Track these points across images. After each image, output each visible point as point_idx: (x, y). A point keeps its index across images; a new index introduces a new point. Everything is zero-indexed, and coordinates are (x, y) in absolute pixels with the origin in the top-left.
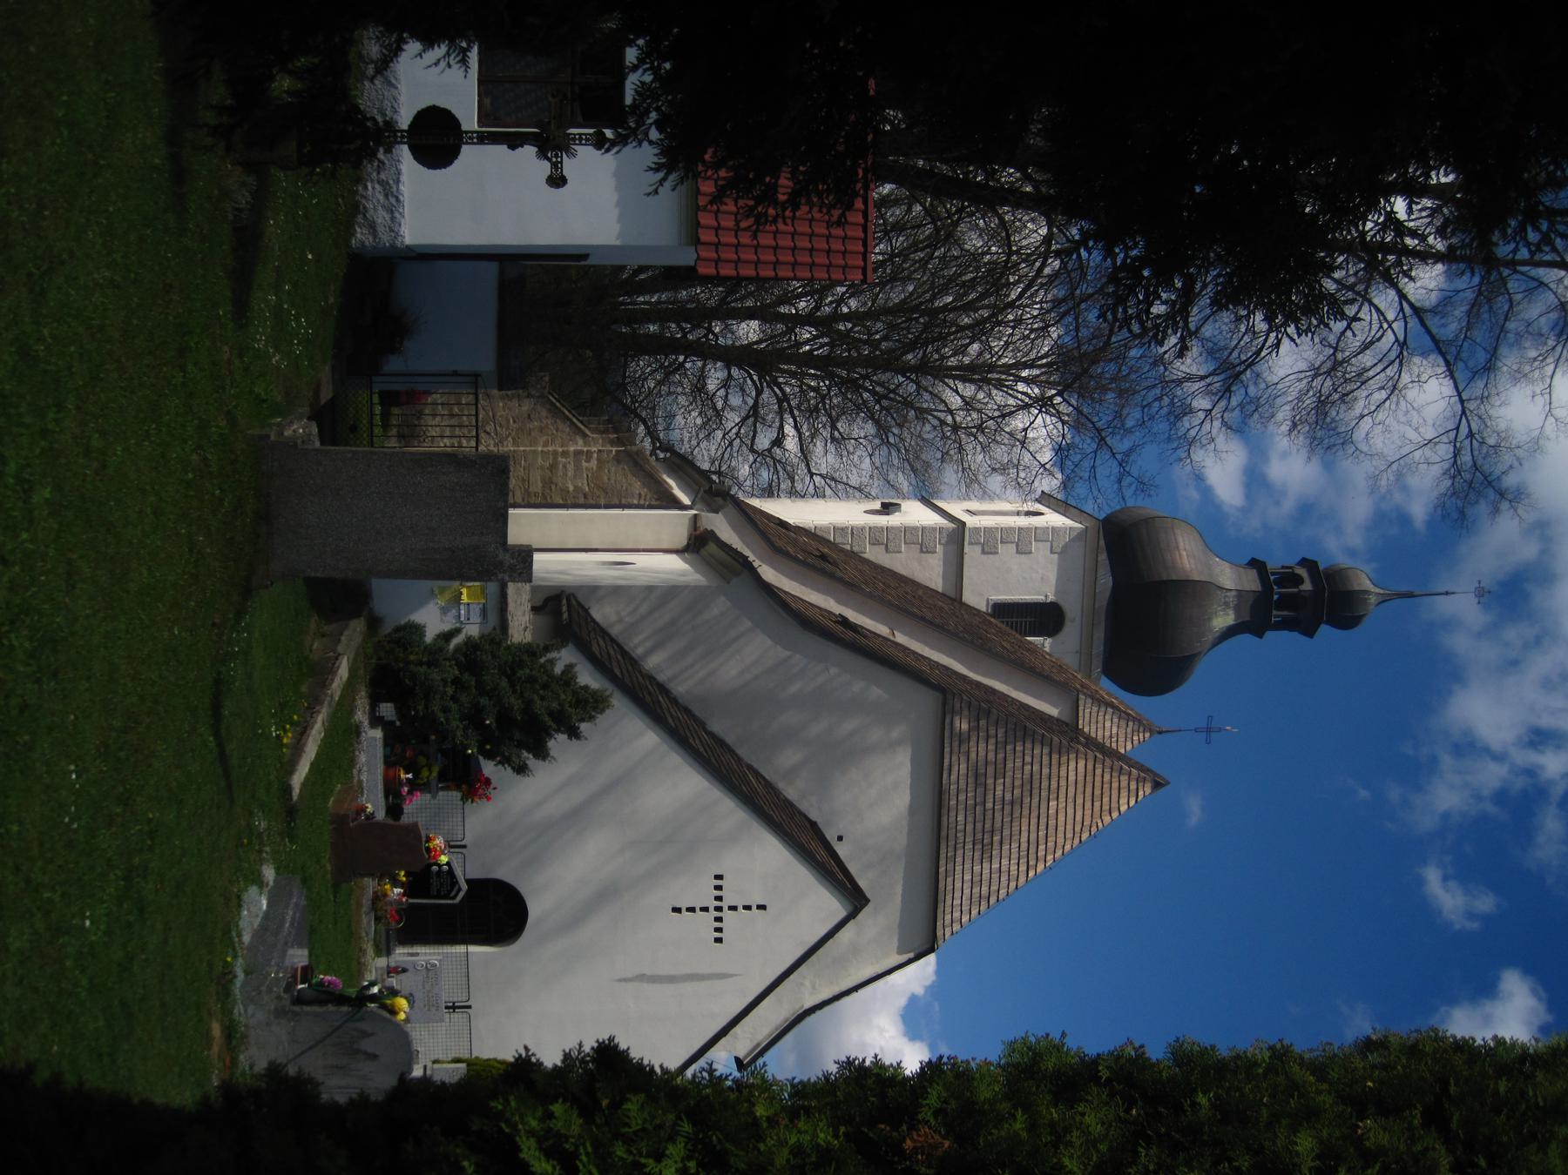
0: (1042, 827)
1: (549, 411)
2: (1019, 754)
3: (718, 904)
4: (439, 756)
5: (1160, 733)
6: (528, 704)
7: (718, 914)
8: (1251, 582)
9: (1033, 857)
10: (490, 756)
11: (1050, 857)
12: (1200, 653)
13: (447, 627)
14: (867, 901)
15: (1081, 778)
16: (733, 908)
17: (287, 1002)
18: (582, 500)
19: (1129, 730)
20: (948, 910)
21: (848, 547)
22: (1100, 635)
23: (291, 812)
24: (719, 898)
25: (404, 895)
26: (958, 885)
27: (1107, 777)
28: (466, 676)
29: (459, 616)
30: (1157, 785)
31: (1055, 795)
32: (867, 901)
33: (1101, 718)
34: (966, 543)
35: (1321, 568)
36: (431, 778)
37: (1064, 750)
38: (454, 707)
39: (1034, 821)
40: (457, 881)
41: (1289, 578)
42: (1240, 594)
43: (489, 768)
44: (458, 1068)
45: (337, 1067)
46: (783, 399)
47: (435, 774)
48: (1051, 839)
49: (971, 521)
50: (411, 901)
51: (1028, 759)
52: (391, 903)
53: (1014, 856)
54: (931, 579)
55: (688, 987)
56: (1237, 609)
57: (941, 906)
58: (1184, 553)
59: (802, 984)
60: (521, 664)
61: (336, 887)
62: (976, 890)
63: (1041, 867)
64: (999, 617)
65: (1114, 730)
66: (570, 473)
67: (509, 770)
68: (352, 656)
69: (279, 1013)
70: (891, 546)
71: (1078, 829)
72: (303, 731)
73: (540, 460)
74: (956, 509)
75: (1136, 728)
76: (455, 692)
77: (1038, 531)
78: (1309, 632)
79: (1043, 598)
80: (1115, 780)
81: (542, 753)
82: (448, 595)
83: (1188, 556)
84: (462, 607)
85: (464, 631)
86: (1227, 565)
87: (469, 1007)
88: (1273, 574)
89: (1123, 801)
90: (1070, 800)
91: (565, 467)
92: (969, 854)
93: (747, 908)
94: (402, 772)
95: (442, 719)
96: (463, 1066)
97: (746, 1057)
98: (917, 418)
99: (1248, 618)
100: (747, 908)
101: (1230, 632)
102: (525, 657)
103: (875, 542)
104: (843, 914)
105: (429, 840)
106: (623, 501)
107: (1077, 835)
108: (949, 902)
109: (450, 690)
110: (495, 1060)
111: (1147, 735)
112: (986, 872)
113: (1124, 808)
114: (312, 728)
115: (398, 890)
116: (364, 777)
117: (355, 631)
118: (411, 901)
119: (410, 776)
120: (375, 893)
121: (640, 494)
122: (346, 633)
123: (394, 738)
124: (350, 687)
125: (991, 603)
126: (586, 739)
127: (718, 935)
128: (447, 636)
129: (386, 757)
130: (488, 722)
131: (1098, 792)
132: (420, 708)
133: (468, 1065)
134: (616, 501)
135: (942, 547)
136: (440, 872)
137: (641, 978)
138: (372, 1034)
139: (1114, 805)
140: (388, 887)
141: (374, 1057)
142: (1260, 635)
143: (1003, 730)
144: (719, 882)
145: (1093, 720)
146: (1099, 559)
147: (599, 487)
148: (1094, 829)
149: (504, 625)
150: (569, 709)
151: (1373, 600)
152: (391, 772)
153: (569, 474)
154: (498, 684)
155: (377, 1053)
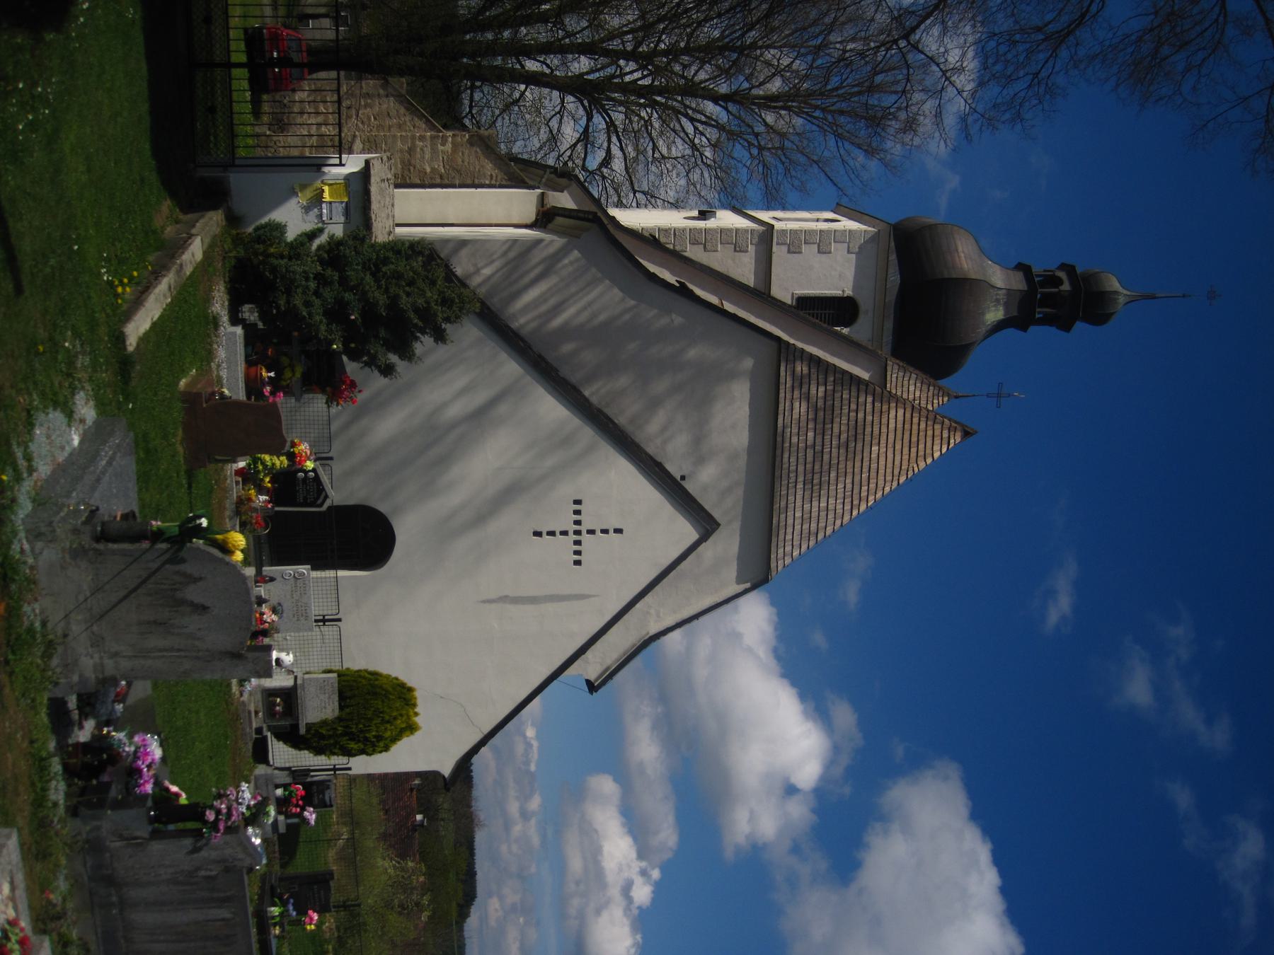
0: (865, 470)
1: (407, 109)
2: (846, 402)
3: (577, 527)
4: (303, 357)
5: (956, 397)
6: (394, 300)
7: (577, 538)
8: (1018, 282)
9: (856, 497)
10: (354, 356)
11: (871, 498)
12: (973, 344)
13: (309, 227)
14: (718, 525)
15: (900, 426)
16: (591, 532)
17: (86, 540)
18: (438, 181)
19: (930, 394)
20: (781, 544)
21: (671, 247)
22: (889, 325)
23: (124, 364)
24: (578, 523)
25: (269, 502)
26: (790, 521)
27: (923, 425)
28: (329, 272)
29: (321, 216)
30: (966, 434)
31: (877, 441)
32: (718, 525)
33: (906, 383)
34: (774, 243)
35: (1078, 272)
36: (294, 379)
37: (885, 399)
38: (317, 302)
39: (858, 464)
40: (323, 489)
41: (1053, 281)
42: (1009, 292)
43: (352, 368)
44: (329, 678)
45: (155, 622)
46: (611, 126)
47: (298, 375)
48: (873, 481)
49: (778, 226)
50: (277, 509)
51: (853, 406)
52: (255, 510)
53: (840, 495)
54: (743, 275)
55: (550, 608)
56: (1007, 306)
57: (774, 539)
58: (962, 255)
59: (648, 613)
60: (386, 261)
61: (190, 475)
62: (806, 526)
63: (863, 507)
64: (806, 310)
65: (917, 394)
66: (427, 156)
67: (376, 372)
68: (207, 241)
69: (78, 553)
70: (709, 246)
71: (896, 472)
72: (144, 290)
73: (399, 143)
74: (765, 216)
75: (936, 392)
76: (318, 287)
77: (837, 234)
78: (1067, 327)
79: (841, 292)
80: (930, 428)
81: (406, 352)
82: (309, 193)
83: (965, 257)
84: (324, 205)
85: (326, 231)
86: (997, 267)
87: (339, 620)
88: (1037, 276)
89: (936, 448)
90: (890, 445)
91: (422, 149)
92: (800, 493)
93: (605, 531)
94: (264, 370)
95: (304, 313)
96: (335, 675)
97: (596, 680)
98: (728, 139)
99: (1015, 314)
100: (605, 531)
101: (999, 326)
102: (390, 254)
103: (694, 242)
104: (694, 536)
105: (293, 445)
106: (476, 181)
107: (896, 478)
108: (781, 537)
109: (312, 285)
110: (366, 671)
111: (946, 399)
112: (815, 509)
113: (937, 455)
114: (155, 287)
115: (263, 498)
116: (224, 374)
117: (213, 221)
118: (277, 509)
119: (272, 374)
120: (239, 497)
121: (491, 175)
122: (201, 221)
123: (252, 337)
124: (205, 266)
125: (795, 296)
126: (452, 342)
127: (577, 557)
128: (312, 235)
129: (247, 356)
130: (353, 317)
131: (914, 439)
132: (282, 302)
133: (339, 676)
134: (469, 182)
135: (754, 247)
136: (306, 478)
137: (504, 599)
138: (201, 579)
139: (929, 451)
140: (252, 492)
141: (204, 609)
142: (1024, 329)
143: (832, 379)
144: (577, 507)
145: (899, 384)
146: (890, 258)
147: (454, 169)
148: (910, 474)
149: (368, 224)
150: (436, 307)
151: (1122, 300)
152: (253, 369)
153: (427, 157)
154: (362, 279)
155: (207, 604)
